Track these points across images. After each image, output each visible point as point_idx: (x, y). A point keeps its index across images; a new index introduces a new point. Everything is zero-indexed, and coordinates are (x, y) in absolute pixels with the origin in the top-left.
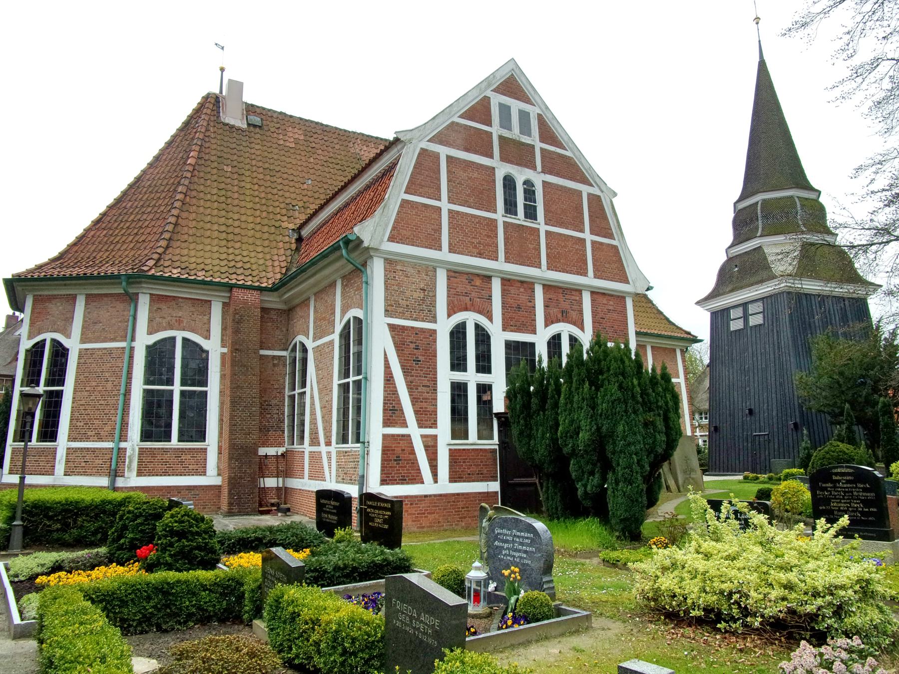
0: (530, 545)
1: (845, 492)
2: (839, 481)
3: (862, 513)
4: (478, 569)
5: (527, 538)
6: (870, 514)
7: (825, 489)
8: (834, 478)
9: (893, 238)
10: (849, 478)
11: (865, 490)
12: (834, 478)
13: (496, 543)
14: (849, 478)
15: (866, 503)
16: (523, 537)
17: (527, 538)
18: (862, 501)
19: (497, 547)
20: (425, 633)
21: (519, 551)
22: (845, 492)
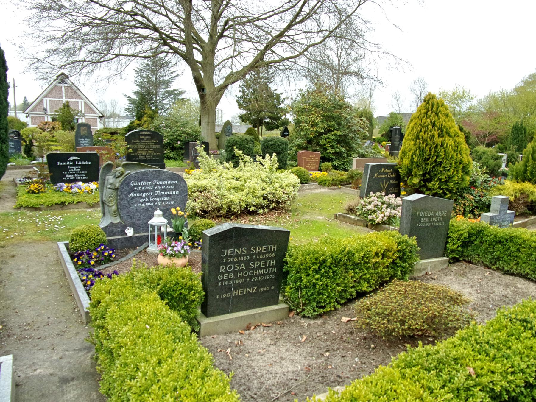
0: (175, 189)
1: (146, 145)
2: (143, 139)
3: (154, 156)
4: (159, 216)
5: (171, 185)
6: (157, 156)
7: (135, 143)
8: (141, 137)
9: (292, 37)
10: (148, 137)
11: (156, 144)
12: (141, 137)
13: (132, 194)
14: (148, 137)
15: (155, 150)
16: (165, 185)
17: (171, 185)
18: (154, 150)
19: (133, 198)
20: (438, 221)
21: (162, 196)
22: (146, 145)
